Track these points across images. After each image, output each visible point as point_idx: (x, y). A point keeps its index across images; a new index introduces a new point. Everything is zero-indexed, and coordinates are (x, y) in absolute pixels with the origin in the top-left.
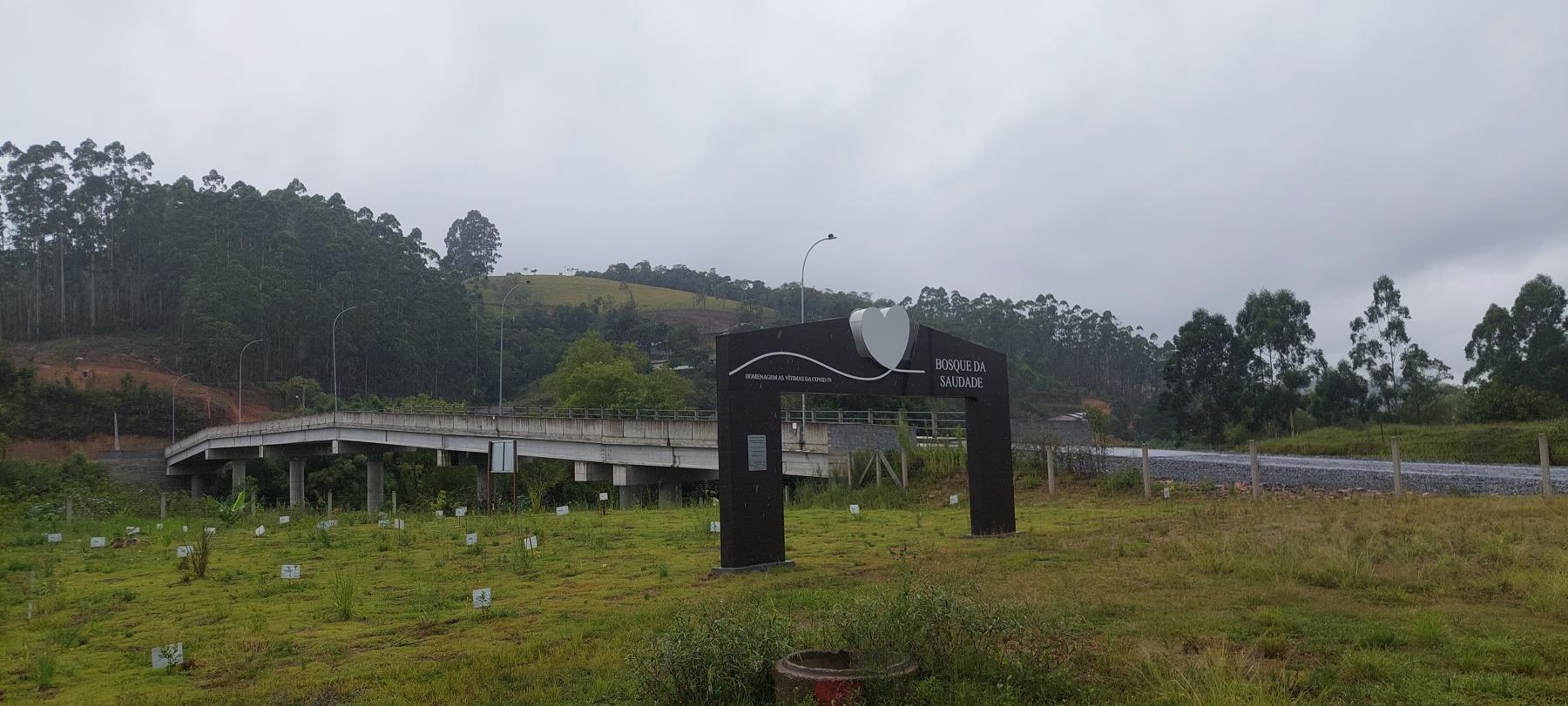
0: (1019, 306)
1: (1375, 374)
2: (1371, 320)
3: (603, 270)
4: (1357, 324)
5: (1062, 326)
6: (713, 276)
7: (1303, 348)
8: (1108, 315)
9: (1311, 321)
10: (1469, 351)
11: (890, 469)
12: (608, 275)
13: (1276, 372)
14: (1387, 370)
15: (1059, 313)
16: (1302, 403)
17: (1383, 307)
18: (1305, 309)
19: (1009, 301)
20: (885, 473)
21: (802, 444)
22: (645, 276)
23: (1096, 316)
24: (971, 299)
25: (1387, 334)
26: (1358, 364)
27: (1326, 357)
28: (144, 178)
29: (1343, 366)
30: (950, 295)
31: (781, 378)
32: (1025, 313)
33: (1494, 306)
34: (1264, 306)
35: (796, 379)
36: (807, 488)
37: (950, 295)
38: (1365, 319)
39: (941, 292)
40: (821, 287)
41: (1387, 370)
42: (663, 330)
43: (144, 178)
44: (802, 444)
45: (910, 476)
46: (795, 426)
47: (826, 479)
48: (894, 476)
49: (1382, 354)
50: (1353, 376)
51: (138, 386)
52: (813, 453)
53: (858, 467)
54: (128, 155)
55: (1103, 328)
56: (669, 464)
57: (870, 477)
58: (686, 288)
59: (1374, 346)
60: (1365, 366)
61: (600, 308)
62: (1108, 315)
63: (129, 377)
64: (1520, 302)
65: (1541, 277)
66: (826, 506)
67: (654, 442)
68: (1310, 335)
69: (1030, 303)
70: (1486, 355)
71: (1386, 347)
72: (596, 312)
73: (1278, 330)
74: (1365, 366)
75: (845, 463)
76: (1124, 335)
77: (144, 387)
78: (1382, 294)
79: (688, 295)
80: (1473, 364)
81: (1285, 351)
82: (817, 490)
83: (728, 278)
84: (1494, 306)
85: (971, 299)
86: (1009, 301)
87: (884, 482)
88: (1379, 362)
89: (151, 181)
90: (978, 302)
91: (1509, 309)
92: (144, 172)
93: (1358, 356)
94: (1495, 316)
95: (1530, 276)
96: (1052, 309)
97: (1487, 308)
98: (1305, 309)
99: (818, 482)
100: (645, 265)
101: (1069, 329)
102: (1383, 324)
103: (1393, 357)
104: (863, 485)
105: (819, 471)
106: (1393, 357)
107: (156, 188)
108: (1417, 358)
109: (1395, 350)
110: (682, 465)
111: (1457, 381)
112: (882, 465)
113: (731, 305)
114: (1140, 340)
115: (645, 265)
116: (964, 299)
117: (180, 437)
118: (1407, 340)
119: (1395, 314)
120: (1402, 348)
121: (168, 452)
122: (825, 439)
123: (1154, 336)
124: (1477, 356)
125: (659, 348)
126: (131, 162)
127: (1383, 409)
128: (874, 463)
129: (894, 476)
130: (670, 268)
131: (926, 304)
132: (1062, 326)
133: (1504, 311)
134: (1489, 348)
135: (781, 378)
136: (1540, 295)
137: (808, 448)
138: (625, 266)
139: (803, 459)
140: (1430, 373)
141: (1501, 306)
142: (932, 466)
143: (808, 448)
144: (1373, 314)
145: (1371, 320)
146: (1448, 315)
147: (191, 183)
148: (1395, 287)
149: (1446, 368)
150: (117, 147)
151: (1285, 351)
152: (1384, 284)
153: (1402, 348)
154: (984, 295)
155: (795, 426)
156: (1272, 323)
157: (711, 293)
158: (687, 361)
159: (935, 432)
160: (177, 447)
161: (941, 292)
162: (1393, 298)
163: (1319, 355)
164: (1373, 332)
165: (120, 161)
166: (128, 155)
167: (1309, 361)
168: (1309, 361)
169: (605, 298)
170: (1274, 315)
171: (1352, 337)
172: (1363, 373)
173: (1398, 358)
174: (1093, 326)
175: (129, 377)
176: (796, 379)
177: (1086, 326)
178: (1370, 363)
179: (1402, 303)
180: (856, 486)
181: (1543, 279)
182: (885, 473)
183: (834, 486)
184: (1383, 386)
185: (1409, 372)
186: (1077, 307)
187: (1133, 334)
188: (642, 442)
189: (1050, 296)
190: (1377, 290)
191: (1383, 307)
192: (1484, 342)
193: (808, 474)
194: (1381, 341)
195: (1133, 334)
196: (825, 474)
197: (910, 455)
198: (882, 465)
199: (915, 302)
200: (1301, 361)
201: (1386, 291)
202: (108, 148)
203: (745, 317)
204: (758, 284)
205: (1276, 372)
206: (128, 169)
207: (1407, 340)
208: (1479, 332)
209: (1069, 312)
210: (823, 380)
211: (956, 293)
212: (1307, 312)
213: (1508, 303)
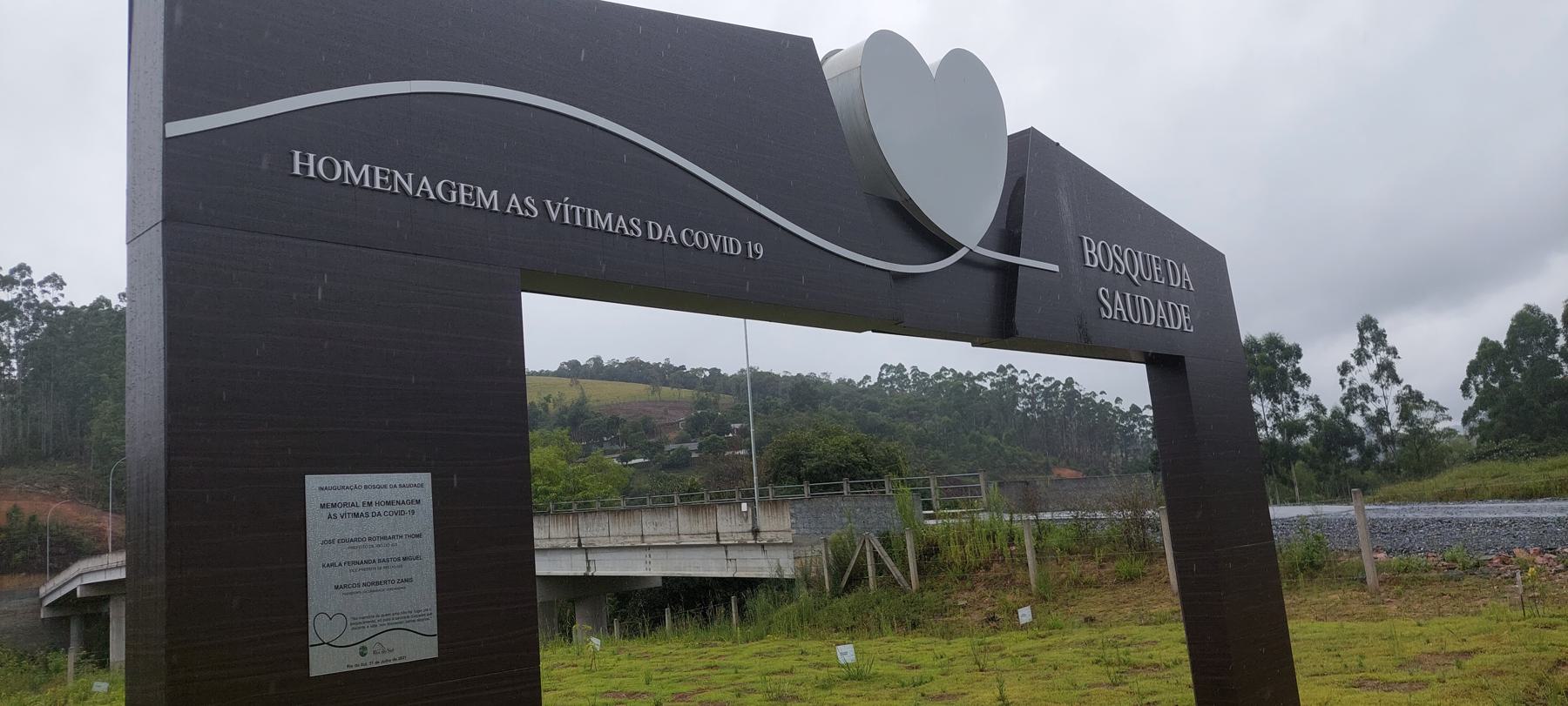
0: (980, 377)
1: (1369, 420)
2: (1360, 363)
3: (554, 368)
4: (1345, 369)
5: (1024, 395)
6: (668, 366)
7: (1296, 395)
8: (1070, 382)
9: (1304, 365)
10: (1465, 389)
11: (889, 562)
12: (560, 373)
13: (1270, 423)
14: (1383, 415)
15: (1020, 382)
16: (1292, 454)
17: (1370, 348)
18: (1296, 353)
19: (969, 373)
20: (881, 569)
21: (756, 532)
22: (597, 371)
23: (1058, 383)
24: (931, 373)
25: (1376, 377)
26: (1351, 409)
27: (1323, 401)
28: (56, 300)
29: (1335, 413)
30: (909, 371)
31: (523, 205)
32: (987, 384)
33: (1485, 340)
34: (1251, 352)
35: (606, 221)
36: (761, 601)
37: (909, 371)
38: (1353, 362)
39: (901, 368)
40: (779, 371)
41: (1383, 415)
42: (615, 422)
43: (56, 300)
44: (756, 532)
45: (920, 570)
46: (744, 506)
47: (791, 582)
48: (896, 573)
49: (1375, 398)
50: (1349, 425)
51: (27, 518)
52: (772, 544)
53: (839, 564)
54: (37, 277)
55: (1066, 395)
56: (581, 572)
57: (858, 577)
58: (639, 380)
59: (1365, 390)
60: (1358, 412)
61: (551, 406)
62: (1070, 382)
63: (16, 509)
64: (1513, 333)
65: (1528, 307)
66: (791, 632)
67: (562, 543)
68: (1304, 379)
69: (991, 374)
70: (1484, 392)
71: (1377, 391)
72: (546, 409)
73: (1269, 377)
74: (1358, 412)
75: (819, 556)
76: (1088, 400)
77: (33, 518)
78: (1367, 335)
79: (642, 387)
80: (1471, 402)
81: (1277, 401)
82: (777, 603)
83: (683, 367)
84: (1485, 340)
85: (931, 373)
86: (969, 373)
87: (880, 585)
88: (1373, 408)
89: (63, 302)
90: (938, 376)
91: (1502, 342)
92: (55, 293)
93: (1349, 400)
94: (1488, 350)
95: (1518, 307)
96: (1013, 379)
97: (1479, 342)
98: (1296, 353)
99: (780, 586)
100: (598, 360)
101: (1032, 398)
102: (1372, 366)
103: (1387, 398)
104: (847, 589)
105: (779, 569)
106: (1387, 398)
107: (70, 310)
108: (1412, 401)
109: (1387, 393)
110: (600, 572)
111: (1456, 424)
112: (876, 555)
113: (686, 394)
114: (1105, 406)
115: (598, 360)
116: (924, 374)
117: (56, 571)
118: (1399, 382)
119: (1383, 354)
120: (1395, 390)
121: (43, 591)
122: (786, 522)
123: (1118, 400)
124: (1475, 395)
125: (611, 442)
126: (41, 284)
127: (1381, 457)
128: (863, 553)
129: (896, 573)
130: (623, 361)
131: (886, 381)
132: (1024, 395)
133: (1497, 344)
134: (1486, 385)
135: (523, 205)
136: (1529, 324)
137: (765, 537)
138: (577, 363)
139: (758, 553)
140: (1426, 415)
141: (1493, 339)
142: (953, 552)
143: (765, 537)
144: (1361, 356)
145: (1360, 363)
146: (1437, 355)
147: (108, 303)
148: (1380, 326)
149: (1442, 409)
150: (23, 269)
151: (1277, 401)
152: (1368, 324)
153: (1395, 390)
154: (944, 369)
155: (744, 506)
156: (1262, 369)
157: (666, 384)
158: (643, 453)
159: (936, 505)
160: (50, 586)
161: (901, 368)
162: (1380, 338)
163: (1315, 401)
164: (1363, 375)
165: (30, 282)
166: (37, 277)
167: (1304, 411)
168: (1304, 411)
169: (555, 395)
170: (1263, 361)
171: (1342, 382)
172: (1356, 419)
173: (1391, 401)
174: (1056, 394)
175: (16, 509)
176: (606, 221)
177: (1049, 394)
178: (1363, 408)
179: (1390, 342)
180: (837, 593)
181: (1530, 309)
182: (881, 569)
183: (803, 593)
184: (1379, 432)
185: (1405, 416)
186: (1038, 375)
187: (1097, 400)
188: (672, 541)
189: (1010, 366)
190: (1361, 331)
191: (1370, 348)
192: (1480, 378)
193: (765, 575)
194: (1372, 384)
195: (1097, 400)
196: (788, 574)
197: (918, 539)
198: (876, 555)
199: (874, 380)
200: (1296, 409)
201: (1370, 331)
202: (13, 271)
203: (702, 404)
204: (715, 372)
205: (1270, 423)
206: (37, 291)
207: (1399, 382)
208: (1473, 369)
209: (1031, 381)
210: (731, 245)
211: (915, 369)
212: (1299, 356)
213: (1500, 337)
